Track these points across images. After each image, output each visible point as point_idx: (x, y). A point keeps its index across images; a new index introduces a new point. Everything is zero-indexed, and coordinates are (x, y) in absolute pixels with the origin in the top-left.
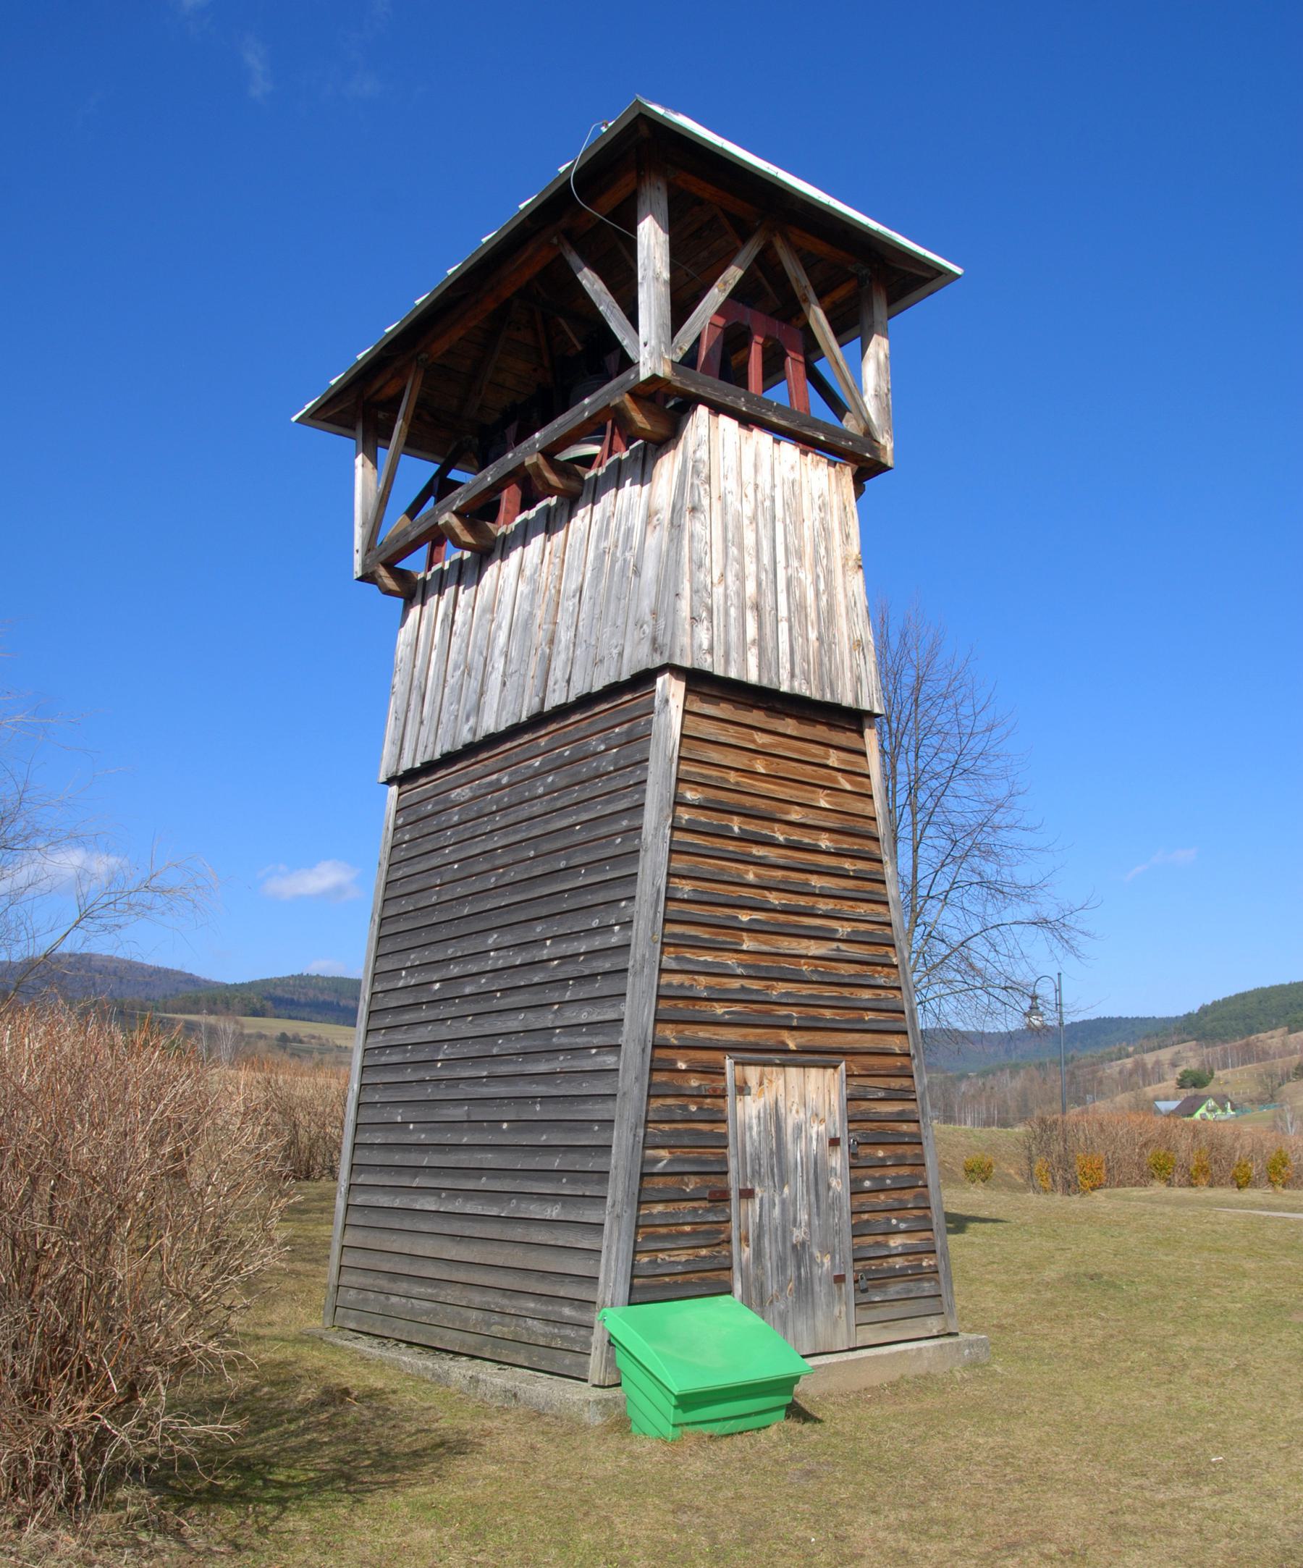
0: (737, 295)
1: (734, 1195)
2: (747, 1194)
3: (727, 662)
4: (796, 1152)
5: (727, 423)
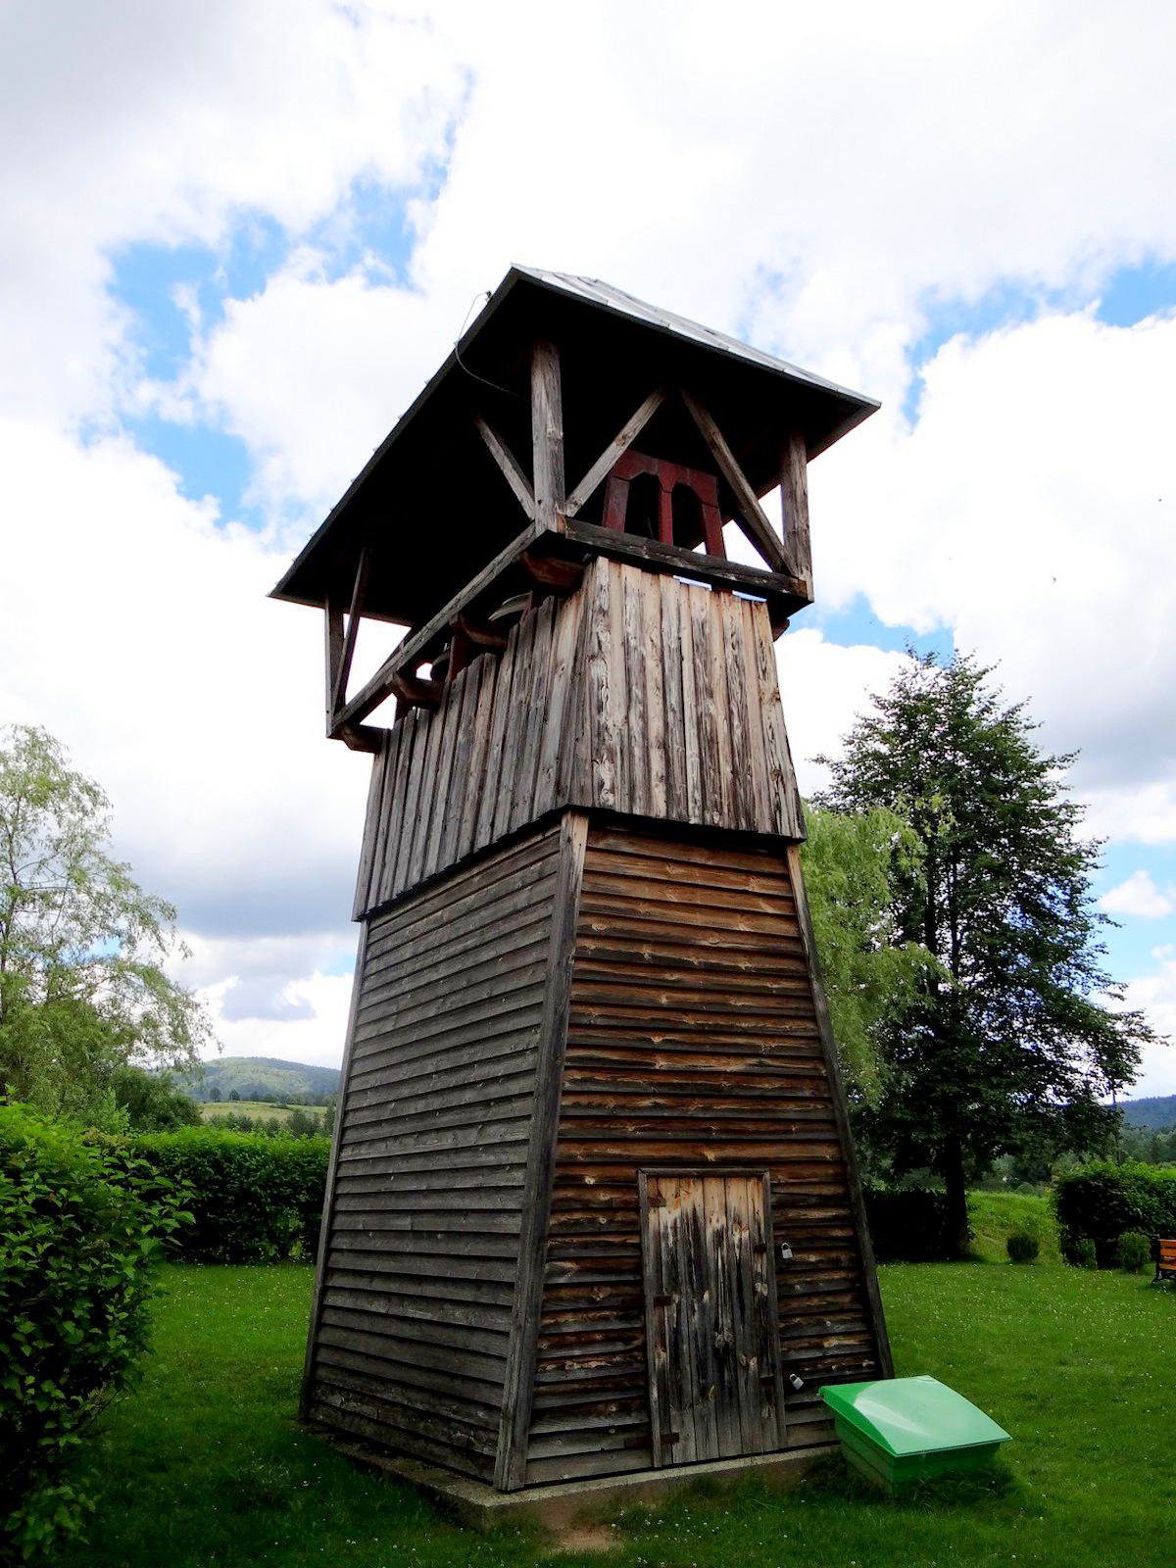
0: (639, 445)
1: (649, 1300)
2: (662, 1302)
3: (632, 799)
4: (716, 1258)
5: (631, 574)
